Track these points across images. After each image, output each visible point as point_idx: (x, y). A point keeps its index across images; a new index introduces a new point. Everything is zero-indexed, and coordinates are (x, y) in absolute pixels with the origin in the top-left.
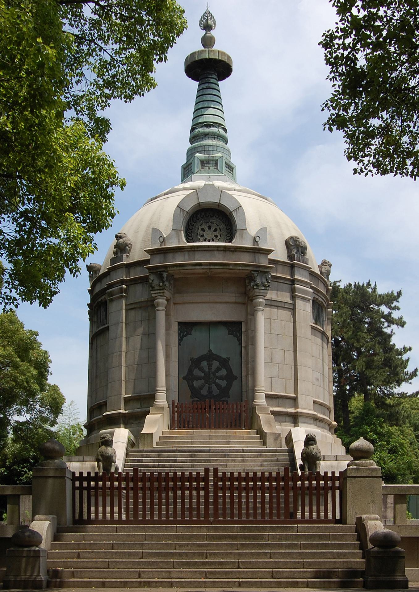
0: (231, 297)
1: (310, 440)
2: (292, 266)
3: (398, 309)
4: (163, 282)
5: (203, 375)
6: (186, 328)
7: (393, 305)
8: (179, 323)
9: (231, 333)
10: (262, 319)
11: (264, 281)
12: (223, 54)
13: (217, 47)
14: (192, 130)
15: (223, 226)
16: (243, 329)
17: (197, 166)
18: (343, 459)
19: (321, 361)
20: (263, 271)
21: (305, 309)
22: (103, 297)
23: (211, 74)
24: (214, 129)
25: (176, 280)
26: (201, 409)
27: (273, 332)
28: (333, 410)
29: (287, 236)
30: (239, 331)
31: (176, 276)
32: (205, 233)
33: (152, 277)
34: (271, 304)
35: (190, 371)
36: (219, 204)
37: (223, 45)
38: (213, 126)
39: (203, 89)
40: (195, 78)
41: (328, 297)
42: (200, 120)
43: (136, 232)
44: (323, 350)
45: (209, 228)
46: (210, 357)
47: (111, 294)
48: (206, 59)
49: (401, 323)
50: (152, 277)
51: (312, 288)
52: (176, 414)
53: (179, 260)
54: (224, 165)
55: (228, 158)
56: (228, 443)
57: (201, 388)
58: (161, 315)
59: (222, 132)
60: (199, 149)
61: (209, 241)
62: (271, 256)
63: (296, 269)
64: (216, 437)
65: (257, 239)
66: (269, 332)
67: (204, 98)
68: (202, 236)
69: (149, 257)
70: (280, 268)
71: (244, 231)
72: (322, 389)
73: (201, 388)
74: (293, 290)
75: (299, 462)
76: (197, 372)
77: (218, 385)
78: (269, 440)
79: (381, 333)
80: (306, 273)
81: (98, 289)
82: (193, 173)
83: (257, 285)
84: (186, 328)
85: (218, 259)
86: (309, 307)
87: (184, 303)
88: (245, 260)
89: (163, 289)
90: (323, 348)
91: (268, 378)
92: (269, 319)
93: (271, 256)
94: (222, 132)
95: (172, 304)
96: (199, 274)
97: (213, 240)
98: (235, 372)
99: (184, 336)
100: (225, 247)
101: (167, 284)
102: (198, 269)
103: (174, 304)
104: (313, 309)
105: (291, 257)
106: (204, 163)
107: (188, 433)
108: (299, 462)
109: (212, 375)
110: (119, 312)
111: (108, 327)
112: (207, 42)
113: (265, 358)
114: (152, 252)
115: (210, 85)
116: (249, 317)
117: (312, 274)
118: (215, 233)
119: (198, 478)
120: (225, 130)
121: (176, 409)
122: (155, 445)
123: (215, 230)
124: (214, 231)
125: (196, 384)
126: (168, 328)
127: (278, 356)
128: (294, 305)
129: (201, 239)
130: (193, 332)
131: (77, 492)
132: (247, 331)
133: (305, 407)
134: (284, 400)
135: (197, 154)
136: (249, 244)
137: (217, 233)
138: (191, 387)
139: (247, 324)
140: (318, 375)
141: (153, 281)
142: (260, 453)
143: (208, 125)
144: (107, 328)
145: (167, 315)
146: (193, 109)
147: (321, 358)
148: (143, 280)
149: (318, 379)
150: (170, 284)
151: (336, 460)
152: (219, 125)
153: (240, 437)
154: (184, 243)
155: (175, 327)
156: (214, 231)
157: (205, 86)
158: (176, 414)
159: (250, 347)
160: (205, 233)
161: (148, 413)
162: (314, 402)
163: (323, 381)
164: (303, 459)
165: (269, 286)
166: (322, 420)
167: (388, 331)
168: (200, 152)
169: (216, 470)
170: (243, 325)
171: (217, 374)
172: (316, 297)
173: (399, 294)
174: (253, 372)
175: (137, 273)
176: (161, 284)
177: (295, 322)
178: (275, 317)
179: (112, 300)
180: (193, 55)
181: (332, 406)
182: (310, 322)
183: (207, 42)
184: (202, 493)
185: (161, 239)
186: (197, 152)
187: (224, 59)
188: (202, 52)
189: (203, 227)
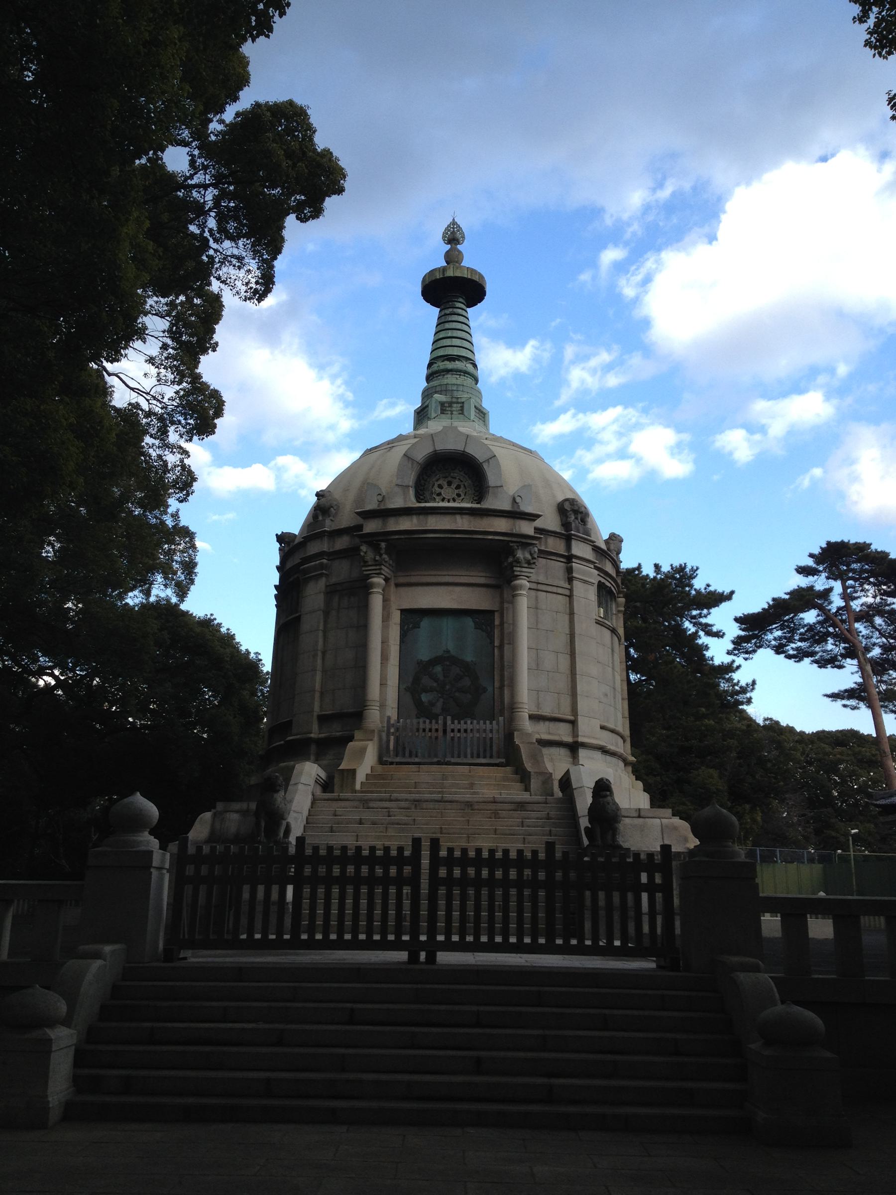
1: (602, 788)
2: (568, 539)
4: (381, 555)
5: (435, 685)
6: (412, 618)
8: (403, 611)
11: (528, 556)
12: (473, 271)
13: (465, 263)
15: (468, 482)
16: (497, 622)
17: (433, 411)
18: (650, 815)
19: (610, 669)
20: (524, 541)
21: (586, 596)
22: (296, 576)
23: (458, 297)
24: (458, 365)
26: (424, 730)
28: (628, 740)
29: (560, 498)
30: (492, 626)
32: (442, 491)
33: (364, 548)
35: (416, 680)
37: (473, 259)
38: (459, 360)
39: (446, 315)
40: (434, 304)
41: (619, 582)
42: (441, 352)
43: (346, 490)
44: (613, 654)
45: (449, 484)
46: (445, 660)
50: (364, 548)
51: (596, 568)
53: (406, 524)
54: (473, 409)
55: (478, 400)
57: (432, 704)
58: (377, 602)
59: (470, 367)
60: (438, 389)
61: (449, 502)
62: (538, 523)
63: (574, 543)
65: (518, 500)
66: (534, 627)
67: (447, 326)
68: (439, 494)
69: (360, 521)
71: (500, 489)
72: (612, 709)
73: (432, 704)
74: (570, 570)
75: (584, 822)
76: (426, 681)
78: (535, 783)
80: (589, 548)
81: (289, 565)
82: (429, 419)
84: (412, 618)
85: (462, 523)
86: (592, 594)
88: (501, 525)
89: (381, 565)
90: (613, 651)
91: (531, 686)
92: (535, 608)
93: (538, 523)
94: (470, 367)
97: (454, 500)
101: (385, 556)
104: (599, 596)
105: (566, 525)
106: (444, 408)
108: (584, 822)
110: (314, 595)
111: (300, 616)
112: (452, 257)
113: (528, 663)
115: (456, 310)
116: (506, 605)
117: (596, 549)
118: (457, 491)
119: (400, 860)
120: (475, 366)
122: (358, 787)
123: (458, 487)
124: (456, 488)
126: (386, 618)
127: (549, 660)
128: (571, 590)
129: (437, 498)
132: (502, 624)
133: (589, 730)
134: (557, 723)
135: (436, 396)
136: (506, 506)
137: (460, 491)
138: (418, 703)
141: (365, 553)
142: (521, 806)
144: (298, 619)
145: (386, 601)
146: (431, 339)
147: (611, 665)
148: (351, 553)
149: (606, 695)
151: (639, 817)
152: (467, 359)
154: (413, 503)
155: (396, 617)
156: (456, 488)
157: (448, 311)
159: (506, 647)
160: (442, 491)
161: (351, 738)
163: (614, 698)
165: (534, 563)
166: (613, 754)
168: (440, 392)
169: (435, 844)
172: (603, 580)
174: (513, 683)
175: (342, 543)
176: (378, 558)
177: (572, 614)
180: (432, 272)
181: (627, 733)
183: (452, 257)
184: (406, 890)
185: (380, 498)
186: (436, 392)
187: (476, 278)
189: (440, 482)
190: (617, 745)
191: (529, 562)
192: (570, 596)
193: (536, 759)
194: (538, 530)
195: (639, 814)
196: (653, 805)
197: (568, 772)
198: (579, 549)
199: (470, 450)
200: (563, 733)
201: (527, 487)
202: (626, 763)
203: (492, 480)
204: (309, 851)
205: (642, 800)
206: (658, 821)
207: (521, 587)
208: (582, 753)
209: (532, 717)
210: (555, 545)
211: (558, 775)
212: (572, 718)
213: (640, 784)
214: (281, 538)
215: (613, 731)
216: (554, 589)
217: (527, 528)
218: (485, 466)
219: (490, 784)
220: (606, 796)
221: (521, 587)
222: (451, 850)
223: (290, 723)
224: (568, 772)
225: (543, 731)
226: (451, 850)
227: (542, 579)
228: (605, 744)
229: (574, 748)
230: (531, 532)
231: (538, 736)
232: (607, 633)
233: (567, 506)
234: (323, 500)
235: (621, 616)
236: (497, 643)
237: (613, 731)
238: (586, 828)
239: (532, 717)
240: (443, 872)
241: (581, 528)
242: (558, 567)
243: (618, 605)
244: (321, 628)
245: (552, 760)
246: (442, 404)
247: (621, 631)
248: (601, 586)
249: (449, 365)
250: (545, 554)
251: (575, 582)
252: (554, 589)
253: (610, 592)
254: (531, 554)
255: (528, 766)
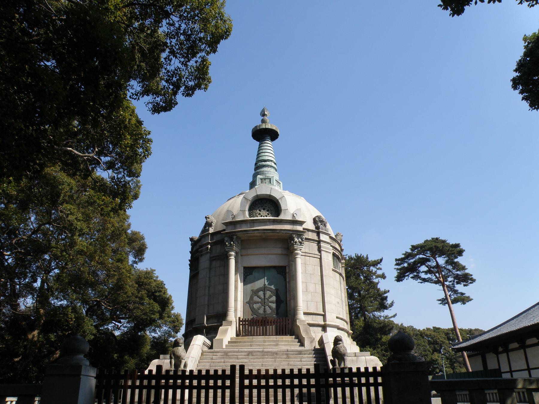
0: (279, 251)
1: (337, 341)
2: (318, 234)
3: (381, 269)
5: (260, 300)
7: (378, 267)
8: (244, 268)
9: (279, 273)
10: (300, 261)
14: (256, 164)
15: (272, 208)
16: (287, 271)
17: (258, 182)
20: (299, 234)
21: (327, 258)
24: (268, 163)
25: (242, 241)
27: (307, 272)
28: (349, 323)
31: (243, 239)
34: (306, 254)
35: (251, 298)
36: (270, 195)
47: (202, 251)
48: (263, 129)
49: (383, 276)
51: (331, 246)
52: (241, 326)
54: (275, 181)
56: (277, 345)
62: (305, 226)
63: (321, 234)
64: (269, 341)
65: (295, 215)
66: (305, 272)
68: (260, 214)
69: (224, 227)
70: (310, 233)
75: (330, 358)
76: (256, 299)
77: (270, 307)
79: (372, 283)
80: (328, 237)
83: (296, 242)
86: (330, 257)
87: (248, 255)
91: (305, 301)
92: (305, 264)
93: (305, 226)
95: (239, 255)
96: (257, 236)
98: (282, 298)
99: (247, 276)
100: (274, 220)
102: (256, 234)
103: (241, 255)
105: (317, 228)
107: (248, 339)
108: (330, 358)
109: (266, 301)
110: (204, 262)
114: (226, 224)
119: (224, 377)
121: (241, 323)
122: (224, 347)
125: (256, 306)
127: (311, 287)
128: (321, 256)
130: (253, 273)
131: (247, 391)
133: (331, 319)
136: (290, 218)
139: (289, 267)
140: (339, 300)
142: (300, 353)
143: (265, 161)
144: (198, 273)
150: (238, 243)
153: (286, 341)
154: (247, 217)
155: (242, 270)
158: (241, 326)
161: (221, 325)
162: (337, 318)
164: (333, 356)
167: (376, 281)
168: (260, 175)
169: (242, 367)
170: (287, 267)
171: (270, 300)
173: (381, 260)
178: (308, 263)
179: (202, 255)
180: (256, 127)
181: (348, 320)
182: (332, 267)
185: (233, 216)
188: (261, 125)
190: (344, 325)
191: (301, 243)
192: (321, 259)
193: (307, 332)
194: (304, 229)
195: (355, 355)
196: (361, 351)
197: (322, 337)
198: (323, 237)
199: (273, 194)
200: (320, 320)
201: (299, 210)
202: (347, 332)
203: (283, 207)
204: (164, 372)
205: (357, 349)
206: (364, 357)
207: (297, 254)
208: (328, 329)
209: (305, 314)
210: (314, 236)
211: (317, 339)
212: (323, 313)
213: (355, 343)
214: (191, 239)
215: (342, 319)
216: (313, 256)
217: (300, 228)
218: (280, 201)
219: (287, 343)
220: (340, 344)
221: (297, 254)
222: (251, 371)
223: (195, 319)
224: (322, 337)
225: (311, 320)
226: (251, 371)
227: (307, 251)
228: (338, 325)
229: (324, 328)
230: (302, 230)
231: (308, 322)
232: (338, 275)
233: (317, 219)
234: (208, 220)
235: (344, 268)
236: (287, 281)
237: (342, 319)
238: (331, 360)
239: (305, 314)
240: (247, 382)
241: (324, 228)
242: (315, 246)
243: (342, 264)
244: (208, 276)
245: (314, 332)
246: (261, 179)
247: (344, 275)
248: (334, 255)
249: (264, 163)
250: (308, 239)
251: (322, 252)
252: (313, 256)
253: (338, 258)
254: (302, 239)
255: (304, 334)
